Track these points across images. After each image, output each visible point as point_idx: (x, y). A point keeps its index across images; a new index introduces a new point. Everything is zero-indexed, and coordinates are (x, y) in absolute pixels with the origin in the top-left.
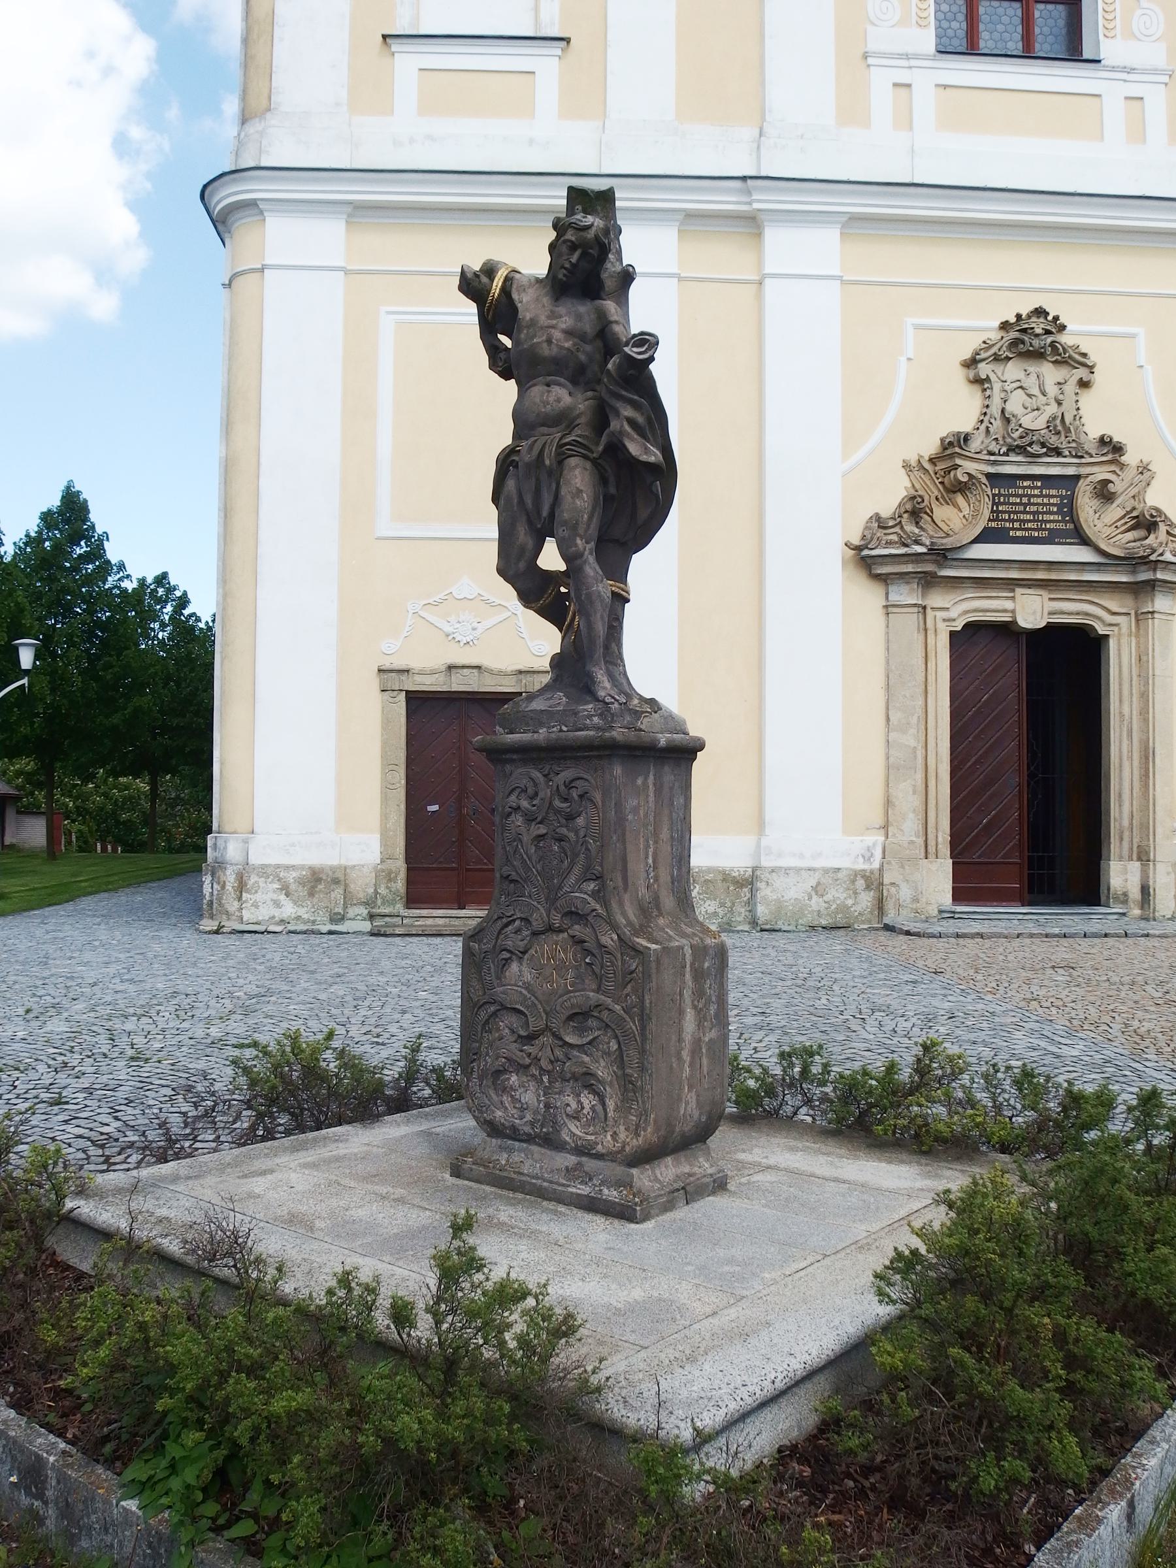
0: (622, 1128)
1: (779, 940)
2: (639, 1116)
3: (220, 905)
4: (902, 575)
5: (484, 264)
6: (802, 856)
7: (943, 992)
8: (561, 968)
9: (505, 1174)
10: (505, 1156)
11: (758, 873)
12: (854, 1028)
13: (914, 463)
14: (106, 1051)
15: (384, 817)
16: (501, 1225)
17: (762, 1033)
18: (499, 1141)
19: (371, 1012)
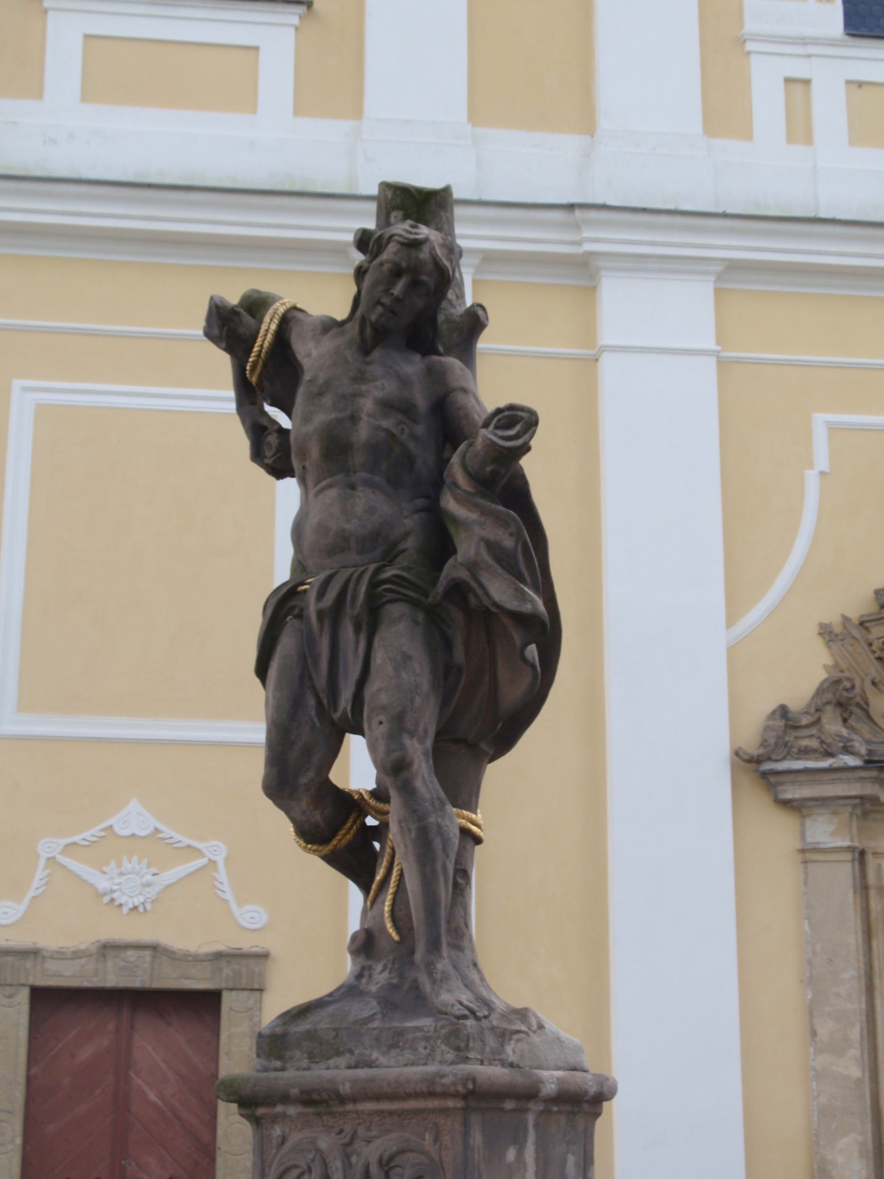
4: (823, 802)
13: (838, 629)
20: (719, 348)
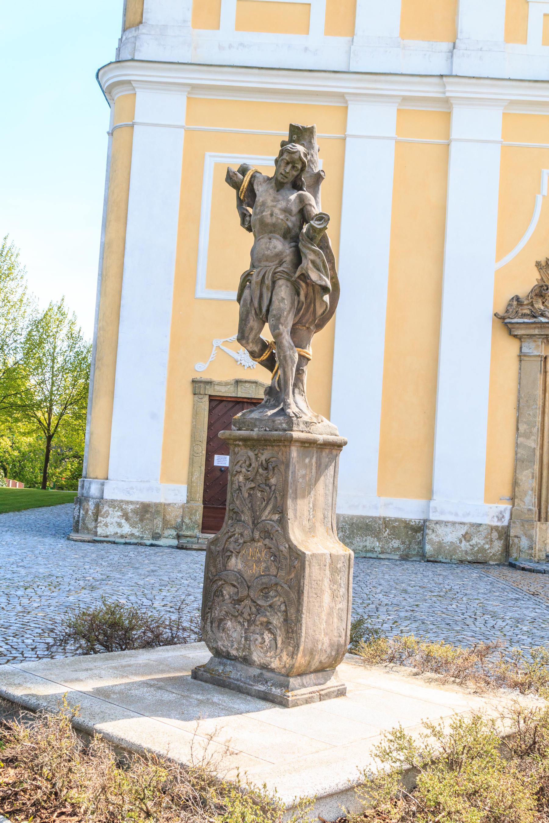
0: (285, 653)
1: (439, 568)
2: (294, 647)
3: (84, 523)
5: (241, 166)
6: (456, 515)
7: (534, 606)
8: (258, 561)
9: (221, 678)
10: (222, 667)
11: (427, 524)
12: (468, 623)
14: (4, 606)
15: (191, 474)
16: (213, 704)
17: (409, 622)
18: (219, 660)
19: (169, 594)
20: (503, 140)
